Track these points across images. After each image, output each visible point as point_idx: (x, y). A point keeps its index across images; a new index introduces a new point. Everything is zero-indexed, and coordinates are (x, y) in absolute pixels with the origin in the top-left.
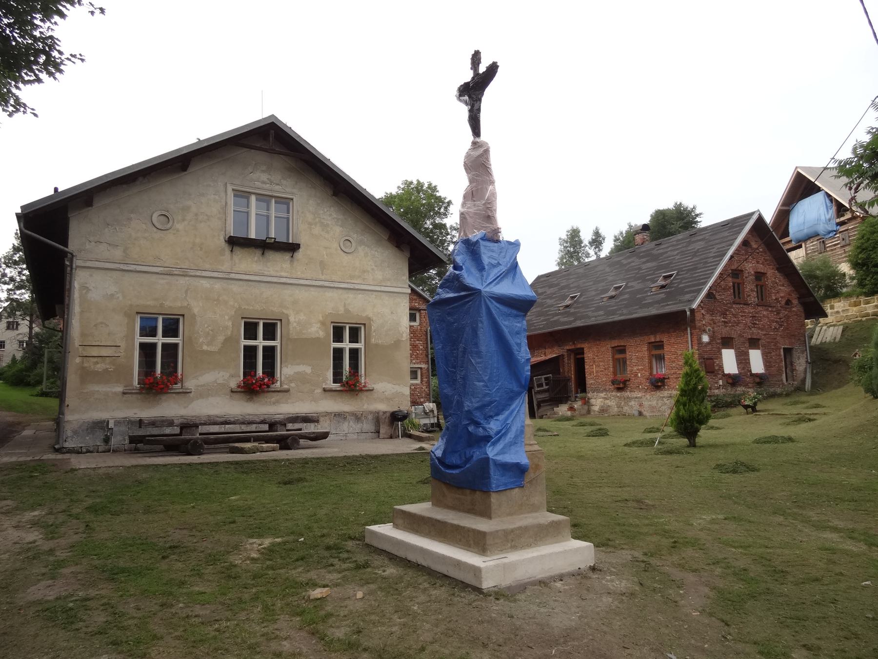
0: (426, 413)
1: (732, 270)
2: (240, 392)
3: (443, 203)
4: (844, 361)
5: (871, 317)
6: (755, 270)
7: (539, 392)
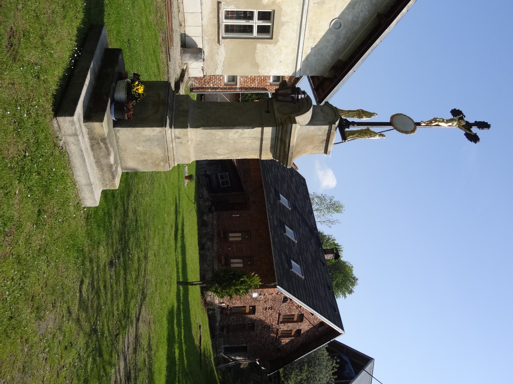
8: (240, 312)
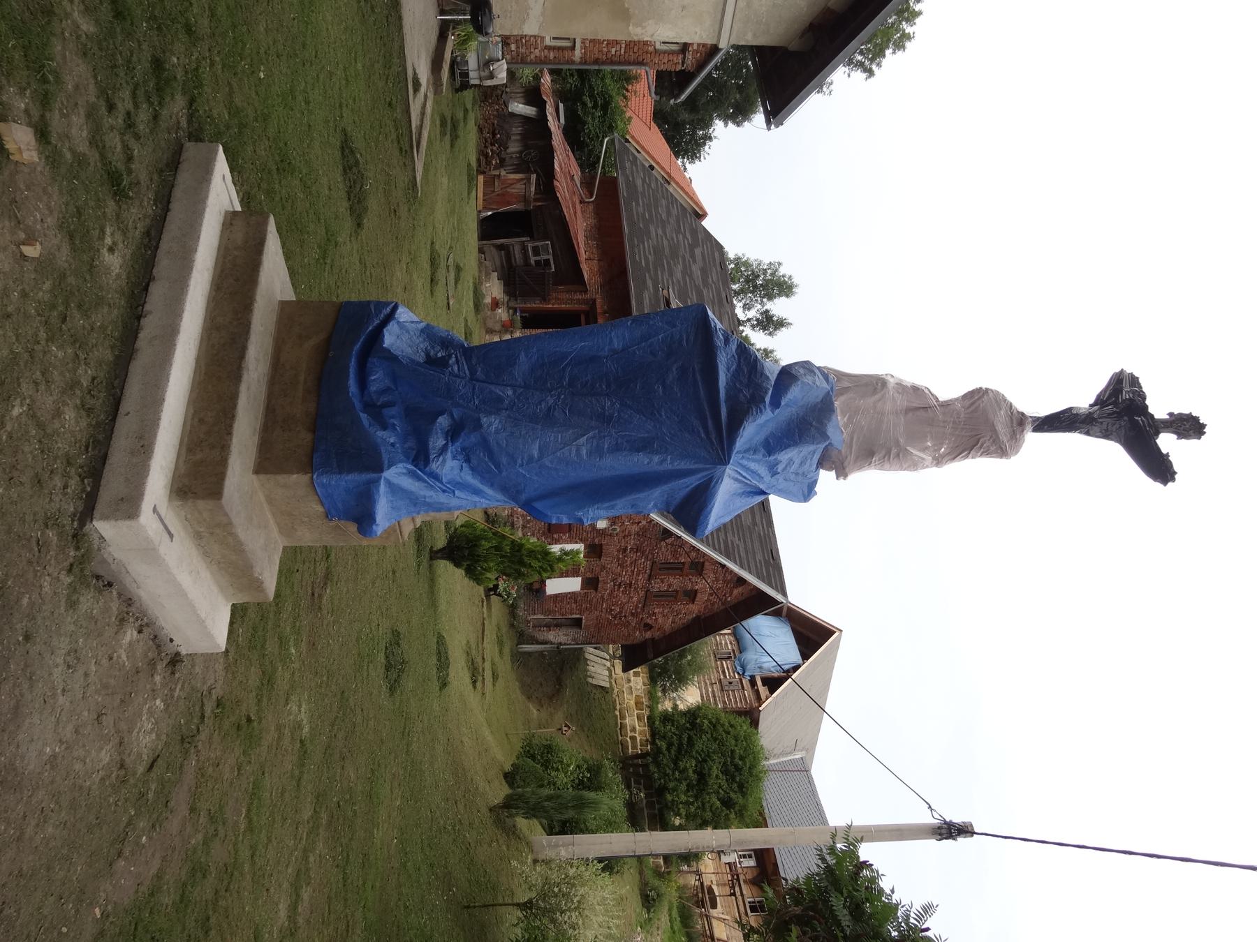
0: (488, 63)
1: (703, 563)
3: (872, 60)
4: (558, 691)
5: (619, 721)
6: (699, 590)
7: (524, 249)
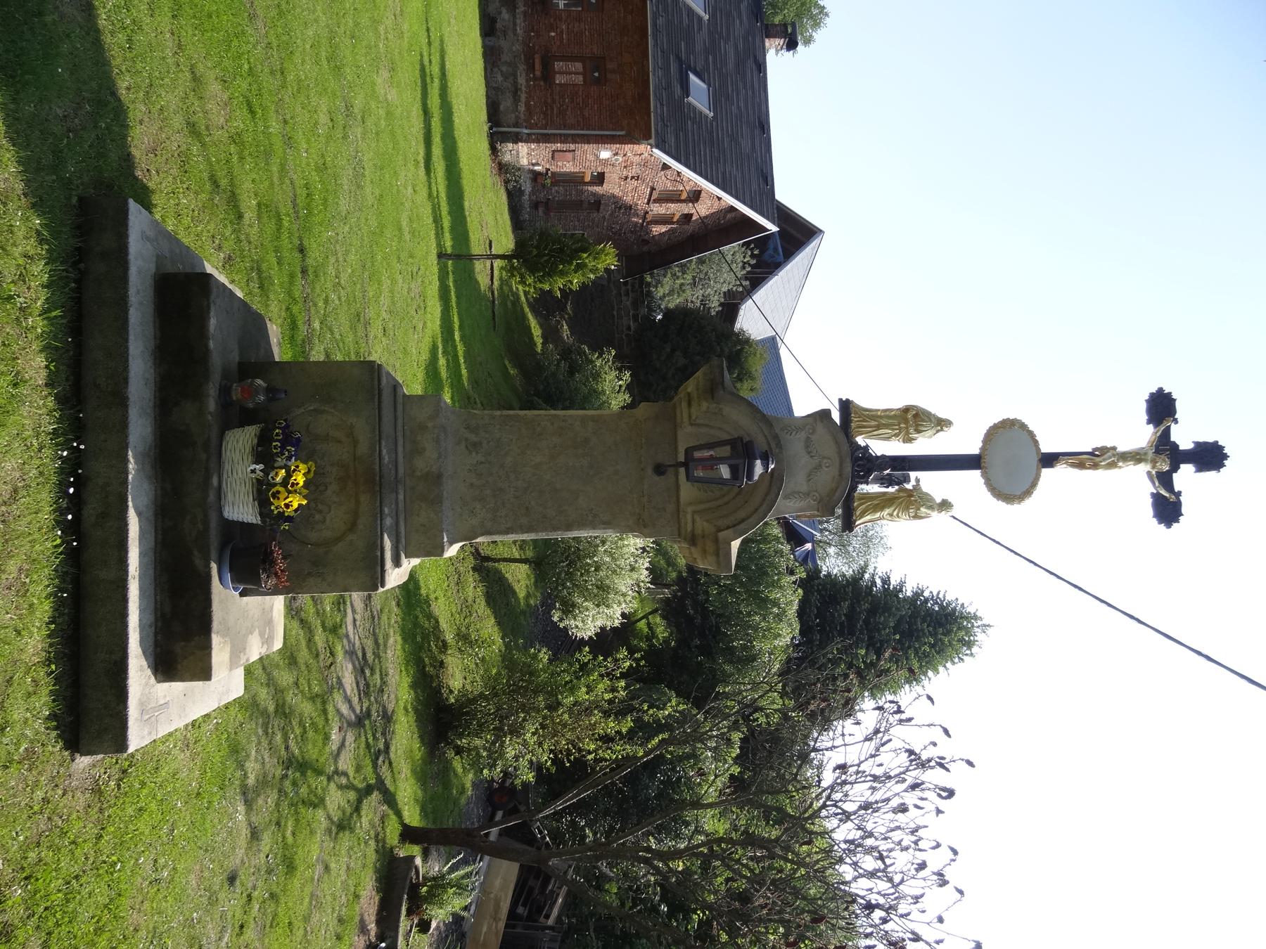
2: (498, 560)
8: (574, 180)
